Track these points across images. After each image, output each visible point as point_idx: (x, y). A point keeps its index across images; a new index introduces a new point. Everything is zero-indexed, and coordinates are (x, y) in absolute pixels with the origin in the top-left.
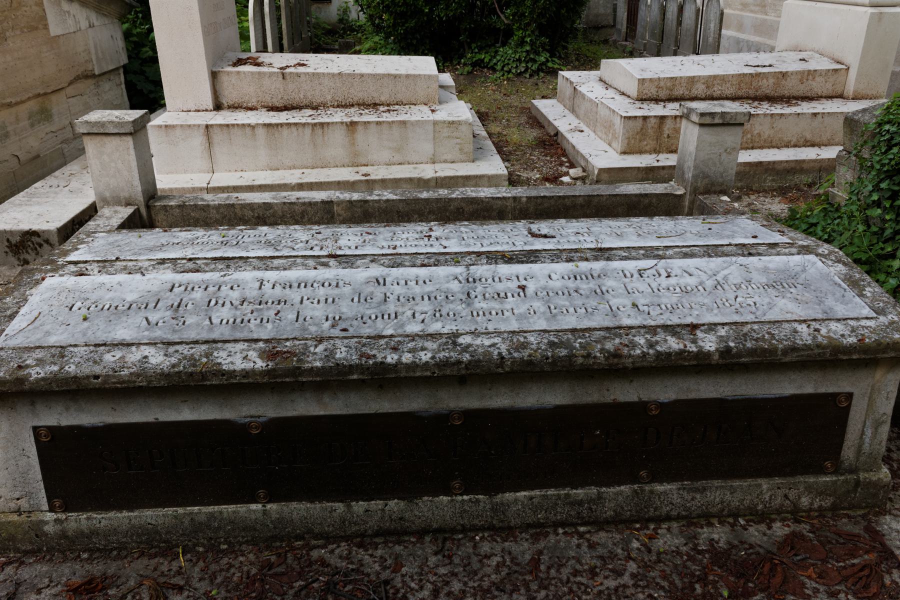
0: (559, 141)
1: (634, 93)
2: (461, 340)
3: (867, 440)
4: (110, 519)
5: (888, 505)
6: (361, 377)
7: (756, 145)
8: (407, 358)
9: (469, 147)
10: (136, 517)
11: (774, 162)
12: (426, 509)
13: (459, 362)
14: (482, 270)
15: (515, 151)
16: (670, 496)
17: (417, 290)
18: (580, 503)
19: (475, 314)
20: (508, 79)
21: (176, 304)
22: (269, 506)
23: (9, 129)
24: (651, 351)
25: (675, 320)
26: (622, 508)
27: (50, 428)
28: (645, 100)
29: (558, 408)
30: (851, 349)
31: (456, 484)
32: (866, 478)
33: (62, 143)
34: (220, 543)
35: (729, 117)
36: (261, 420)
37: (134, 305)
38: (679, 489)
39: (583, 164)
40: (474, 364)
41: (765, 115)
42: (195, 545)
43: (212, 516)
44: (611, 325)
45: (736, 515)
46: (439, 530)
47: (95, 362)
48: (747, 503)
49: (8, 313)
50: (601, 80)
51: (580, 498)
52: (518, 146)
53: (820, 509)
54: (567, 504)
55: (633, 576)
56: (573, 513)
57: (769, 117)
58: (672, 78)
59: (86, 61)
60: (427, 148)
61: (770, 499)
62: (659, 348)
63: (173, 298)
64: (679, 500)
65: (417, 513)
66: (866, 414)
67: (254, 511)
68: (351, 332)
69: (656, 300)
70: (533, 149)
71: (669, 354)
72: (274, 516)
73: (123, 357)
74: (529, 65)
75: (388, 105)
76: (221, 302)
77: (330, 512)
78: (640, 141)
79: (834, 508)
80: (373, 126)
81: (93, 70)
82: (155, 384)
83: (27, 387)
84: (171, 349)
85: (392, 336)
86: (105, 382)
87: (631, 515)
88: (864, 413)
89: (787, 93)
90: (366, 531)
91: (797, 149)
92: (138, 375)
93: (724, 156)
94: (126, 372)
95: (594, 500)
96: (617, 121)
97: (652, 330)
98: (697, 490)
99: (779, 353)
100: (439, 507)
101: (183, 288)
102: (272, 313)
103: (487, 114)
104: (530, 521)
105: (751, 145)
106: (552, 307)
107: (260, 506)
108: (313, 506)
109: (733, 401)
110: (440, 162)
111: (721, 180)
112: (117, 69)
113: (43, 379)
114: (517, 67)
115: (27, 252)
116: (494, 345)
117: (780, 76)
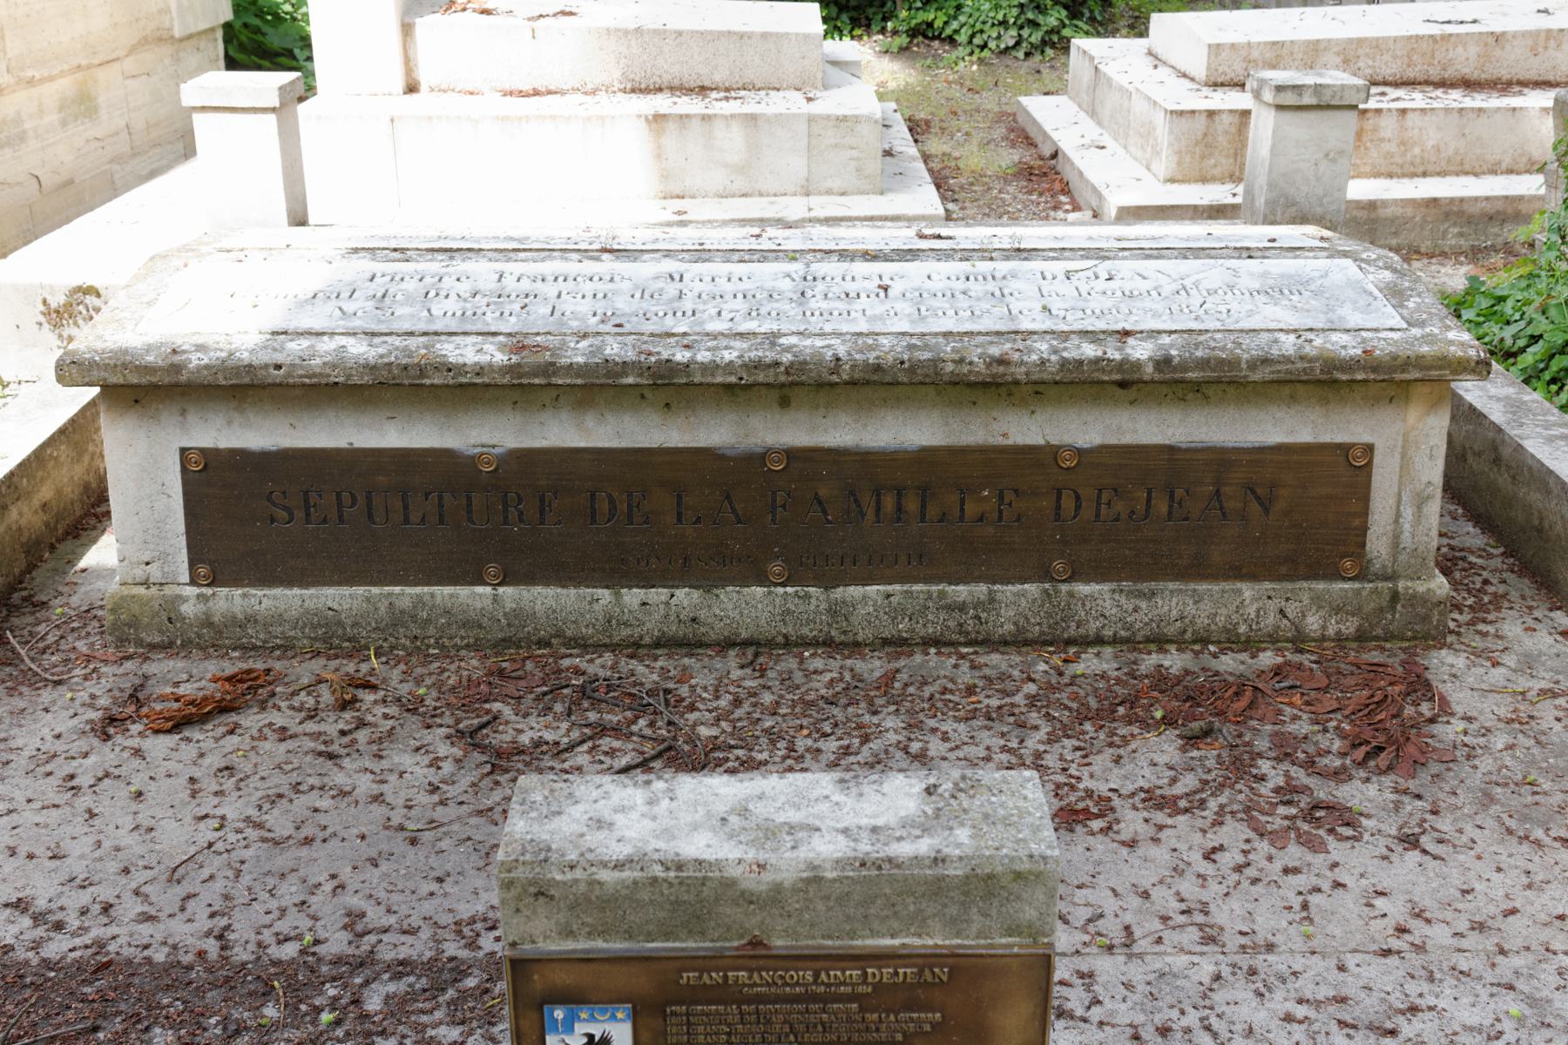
0: (1059, 168)
1: (1200, 72)
2: (783, 341)
3: (1407, 526)
4: (275, 598)
5: (1449, 639)
6: (639, 380)
7: (1430, 168)
8: (703, 356)
9: (875, 164)
10: (311, 597)
11: (1462, 200)
12: (731, 606)
13: (777, 364)
14: (831, 267)
15: (972, 184)
16: (1100, 602)
17: (729, 288)
18: (962, 607)
19: (808, 313)
20: (981, 61)
21: (379, 295)
22: (501, 590)
23: (27, 126)
24: (1054, 358)
25: (1101, 325)
26: (1027, 619)
27: (203, 451)
28: (1222, 85)
29: (924, 450)
30: (1351, 365)
31: (776, 568)
32: (1407, 588)
33: (111, 161)
34: (428, 646)
35: (1328, 93)
36: (497, 451)
37: (320, 295)
38: (1114, 591)
39: (1094, 204)
40: (799, 366)
41: (1447, 110)
42: (393, 648)
43: (419, 601)
44: (1004, 328)
45: (1205, 641)
46: (746, 643)
47: (275, 350)
48: (1220, 620)
49: (145, 299)
50: (1150, 53)
51: (961, 599)
52: (978, 176)
53: (1340, 639)
54: (943, 608)
55: (1028, 697)
56: (952, 624)
57: (1456, 115)
58: (1274, 43)
59: (160, 11)
60: (795, 166)
61: (1258, 616)
62: (1065, 354)
63: (378, 287)
64: (1114, 611)
65: (718, 612)
66: (1400, 483)
67: (480, 595)
68: (628, 328)
69: (1081, 304)
70: (1006, 180)
71: (1080, 363)
72: (509, 605)
73: (312, 346)
74: (1025, 32)
75: (727, 90)
76: (443, 293)
77: (590, 603)
78: (1203, 157)
79: (1361, 637)
80: (695, 123)
81: (170, 29)
82: (356, 380)
83: (183, 378)
84: (377, 340)
85: (685, 334)
86: (289, 375)
87: (1042, 633)
88: (1396, 478)
89: (1505, 75)
90: (641, 638)
91: (1513, 177)
92: (334, 366)
93: (1324, 165)
94: (318, 361)
95: (983, 603)
96: (1160, 120)
97: (1064, 336)
98: (1141, 595)
99: (1244, 366)
100: (747, 605)
101: (388, 278)
102: (516, 307)
103: (927, 123)
104: (886, 634)
105: (1421, 169)
106: (923, 309)
107: (488, 589)
108: (565, 591)
109: (1188, 450)
110: (820, 193)
111: (1319, 210)
112: (212, 30)
113: (207, 367)
114: (999, 37)
115: (76, 324)
116: (829, 346)
117: (1491, 40)
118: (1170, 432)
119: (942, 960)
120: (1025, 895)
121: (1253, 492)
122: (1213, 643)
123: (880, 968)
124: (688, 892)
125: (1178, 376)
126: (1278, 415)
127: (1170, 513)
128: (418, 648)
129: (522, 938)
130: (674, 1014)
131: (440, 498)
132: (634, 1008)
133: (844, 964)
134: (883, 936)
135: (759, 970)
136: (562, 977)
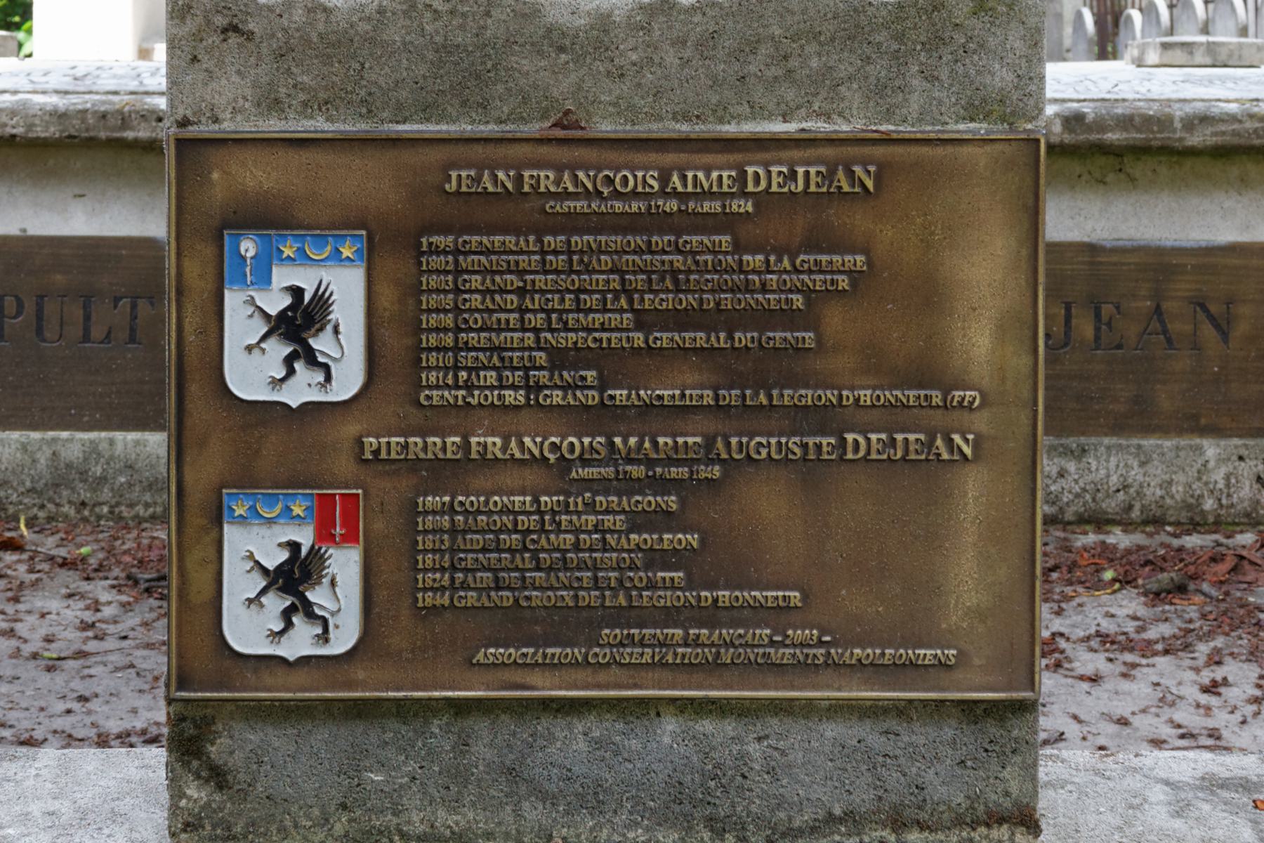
48: (1178, 490)
61: (1228, 486)
82: (39, 132)
98: (1067, 452)
99: (1178, 125)
109: (1114, 250)
118: (1089, 225)
119: (867, 150)
120: (992, 42)
121: (1203, 307)
122: (1170, 524)
123: (766, 165)
124: (462, 27)
125: (1094, 137)
126: (1227, 204)
127: (1097, 338)
128: (85, 520)
129: (199, 112)
130: (435, 251)
131: (134, 306)
132: (370, 238)
133: (708, 158)
134: (770, 117)
135: (573, 168)
136: (256, 176)
